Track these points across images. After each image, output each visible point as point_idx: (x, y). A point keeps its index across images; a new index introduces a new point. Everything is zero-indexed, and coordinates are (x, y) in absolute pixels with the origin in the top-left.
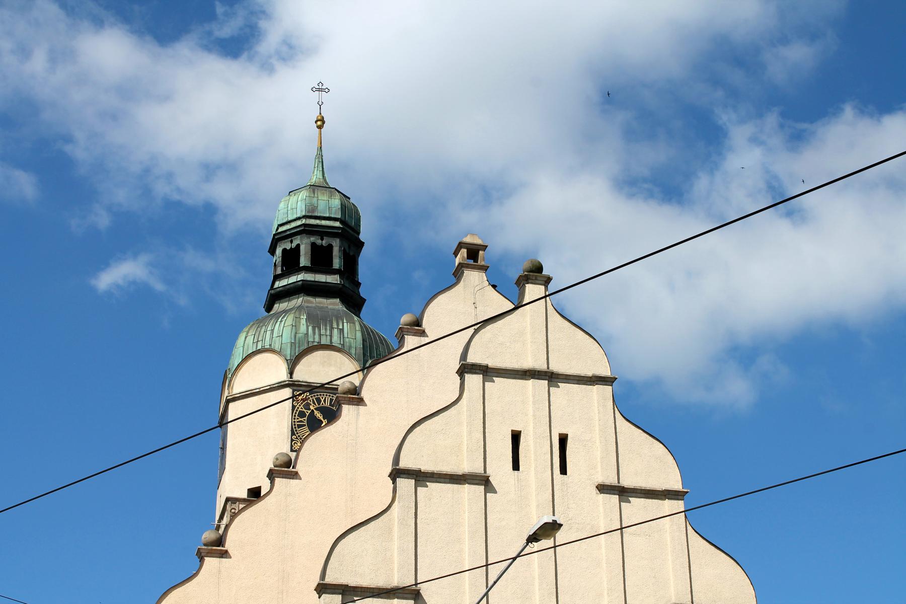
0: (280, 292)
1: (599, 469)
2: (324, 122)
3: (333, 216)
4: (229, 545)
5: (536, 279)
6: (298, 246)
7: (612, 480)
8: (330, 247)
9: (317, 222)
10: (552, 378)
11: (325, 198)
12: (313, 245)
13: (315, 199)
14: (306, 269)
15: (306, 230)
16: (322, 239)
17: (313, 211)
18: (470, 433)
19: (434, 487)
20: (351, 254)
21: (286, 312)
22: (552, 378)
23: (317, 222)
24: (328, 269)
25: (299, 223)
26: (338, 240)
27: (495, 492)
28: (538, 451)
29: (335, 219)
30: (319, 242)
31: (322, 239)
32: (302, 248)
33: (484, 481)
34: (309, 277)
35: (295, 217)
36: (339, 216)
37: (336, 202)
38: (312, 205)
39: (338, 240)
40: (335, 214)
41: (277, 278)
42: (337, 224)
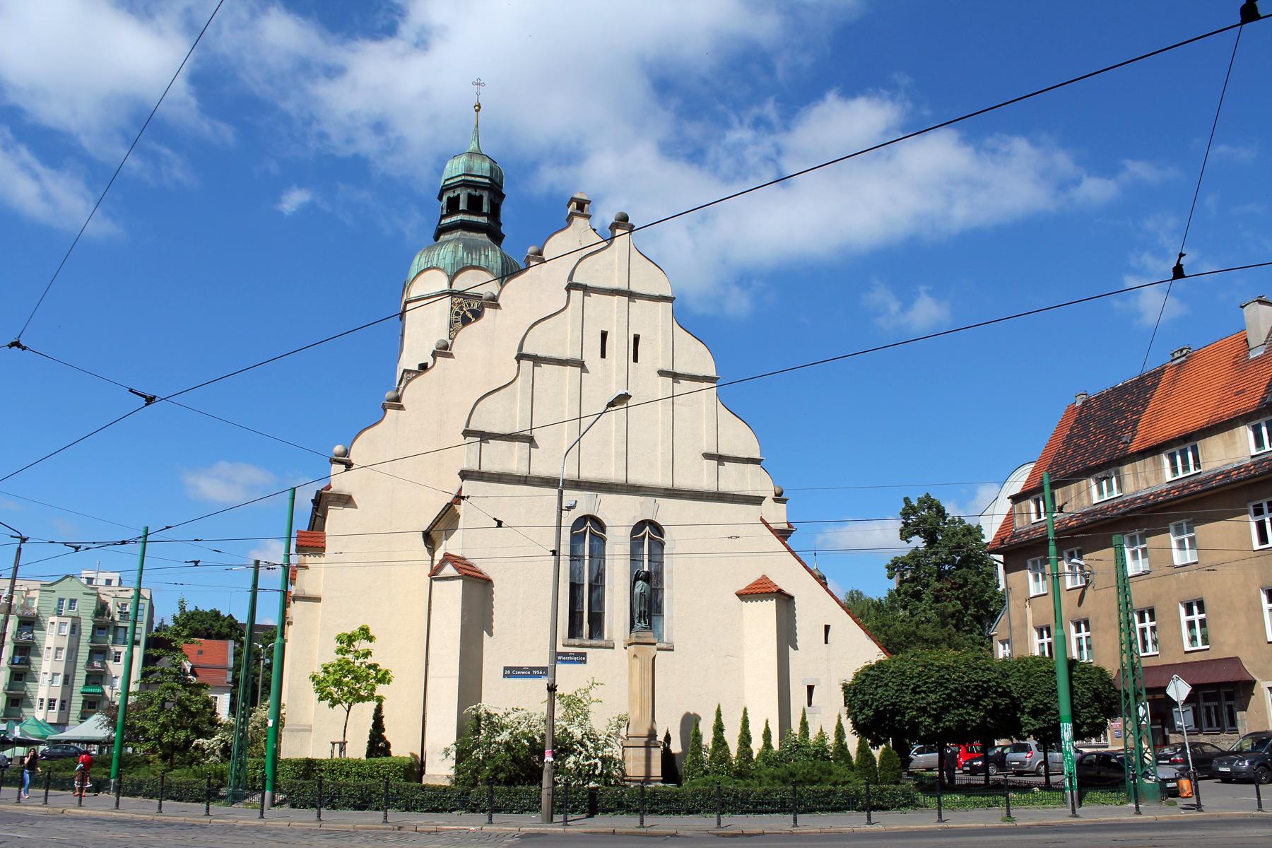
4: (403, 402)
7: (668, 368)
8: (481, 197)
10: (631, 295)
12: (469, 195)
14: (464, 212)
15: (465, 184)
22: (631, 295)
33: (581, 365)
37: (487, 165)
41: (443, 217)
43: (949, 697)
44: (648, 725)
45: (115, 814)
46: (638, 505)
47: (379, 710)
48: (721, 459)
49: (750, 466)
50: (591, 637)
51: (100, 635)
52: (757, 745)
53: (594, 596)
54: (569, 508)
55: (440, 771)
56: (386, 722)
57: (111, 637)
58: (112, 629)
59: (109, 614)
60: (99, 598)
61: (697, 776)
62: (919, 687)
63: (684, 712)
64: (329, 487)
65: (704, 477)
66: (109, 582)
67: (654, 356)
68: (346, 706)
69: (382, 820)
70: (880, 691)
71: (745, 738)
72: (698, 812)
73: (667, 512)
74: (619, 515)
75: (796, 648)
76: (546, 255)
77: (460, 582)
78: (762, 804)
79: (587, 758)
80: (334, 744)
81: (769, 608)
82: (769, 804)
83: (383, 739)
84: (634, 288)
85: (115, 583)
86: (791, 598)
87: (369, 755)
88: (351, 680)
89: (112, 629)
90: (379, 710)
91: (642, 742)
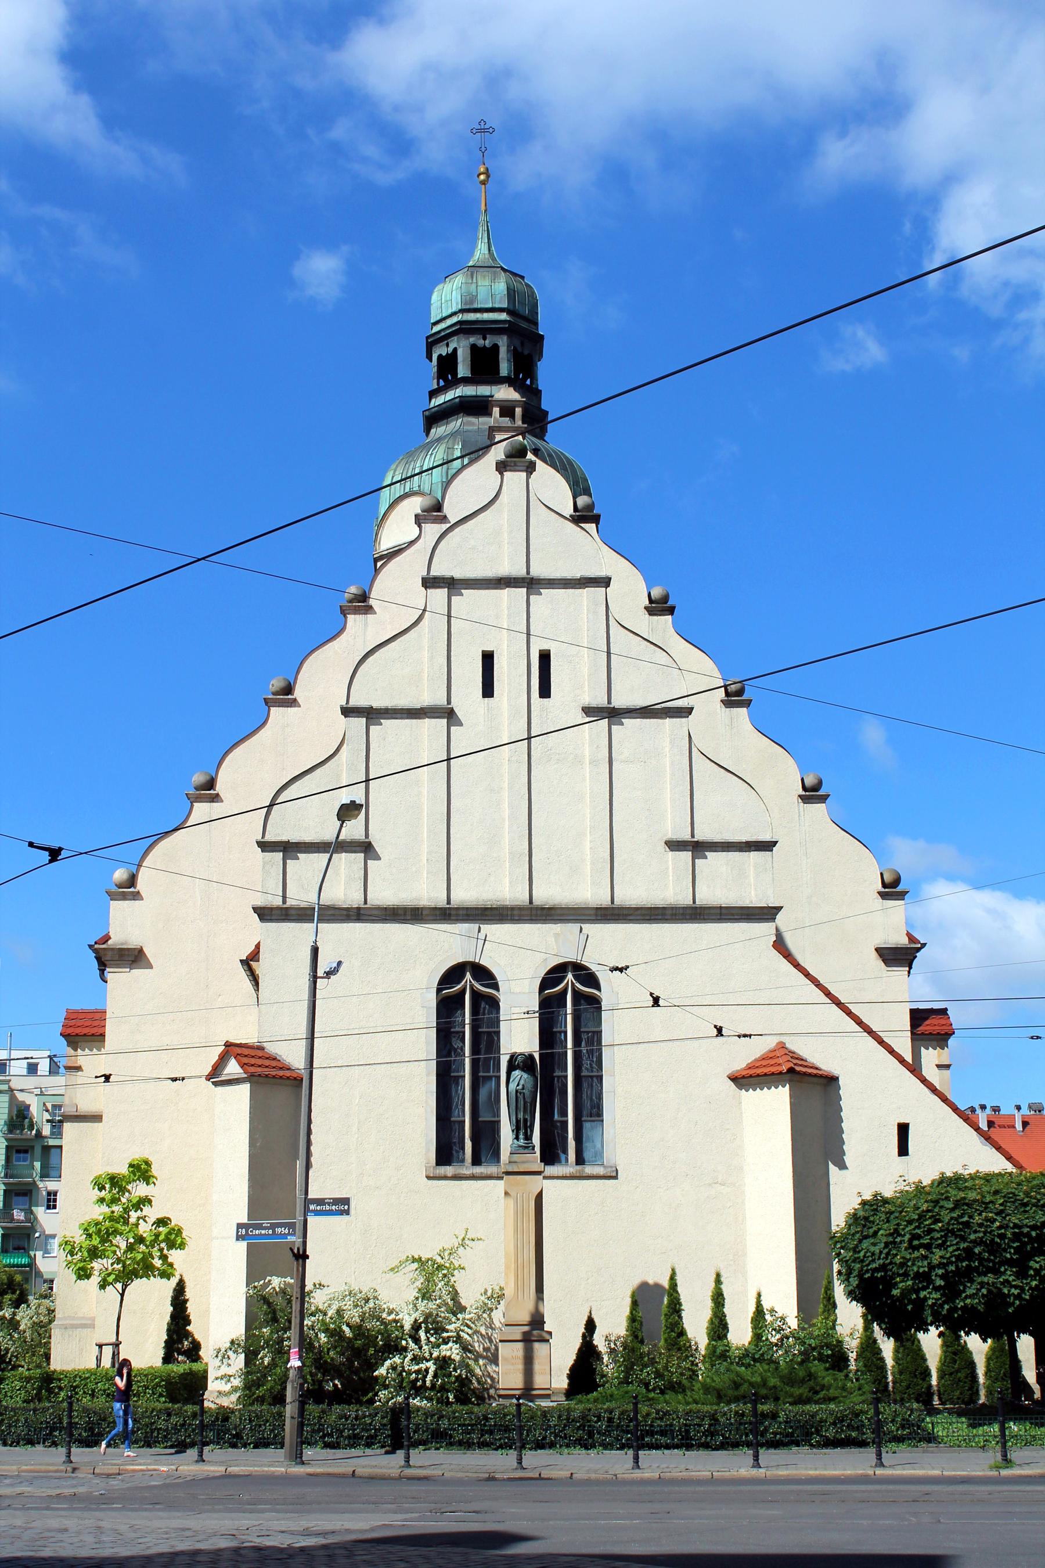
0: (437, 412)
1: (586, 689)
2: (488, 176)
3: (497, 306)
4: (220, 787)
5: (515, 465)
6: (455, 350)
7: (601, 701)
8: (496, 348)
9: (478, 316)
10: (531, 584)
11: (487, 283)
12: (474, 348)
13: (474, 286)
14: (465, 381)
15: (464, 329)
16: (485, 339)
17: (472, 302)
18: (431, 658)
19: (389, 724)
20: (526, 352)
21: (439, 440)
22: (531, 584)
23: (478, 316)
24: (495, 379)
25: (455, 319)
26: (505, 338)
27: (461, 724)
28: (512, 674)
29: (501, 310)
30: (480, 343)
31: (485, 339)
32: (460, 352)
33: (449, 714)
34: (469, 391)
35: (449, 312)
36: (505, 305)
37: (501, 287)
38: (470, 294)
39: (505, 338)
40: (500, 302)
41: (433, 394)
42: (504, 316)
43: (969, 1254)
44: (529, 1305)
45: (754, 1472)
46: (551, 940)
47: (180, 1290)
48: (698, 848)
49: (754, 856)
50: (476, 1161)
51: (19, 1163)
52: (740, 1335)
53: (483, 1092)
54: (329, 974)
55: (223, 1385)
56: (191, 1308)
57: (37, 1165)
58: (38, 1150)
59: (31, 1126)
60: (13, 1099)
61: (653, 1386)
62: (917, 1237)
63: (636, 1282)
64: (106, 938)
65: (666, 881)
66: (32, 1069)
67: (577, 683)
68: (119, 1286)
69: (64, 1458)
70: (865, 1244)
71: (719, 1327)
72: (552, 1445)
73: (600, 946)
74: (517, 963)
75: (842, 1166)
76: (453, 510)
77: (245, 1089)
78: (651, 1433)
79: (416, 1360)
80: (100, 1346)
81: (776, 1102)
82: (663, 1433)
83: (188, 1335)
84: (536, 571)
85: (44, 1066)
86: (831, 1081)
87: (167, 1359)
88: (133, 1247)
89: (38, 1150)
90: (180, 1290)
91: (517, 1333)
